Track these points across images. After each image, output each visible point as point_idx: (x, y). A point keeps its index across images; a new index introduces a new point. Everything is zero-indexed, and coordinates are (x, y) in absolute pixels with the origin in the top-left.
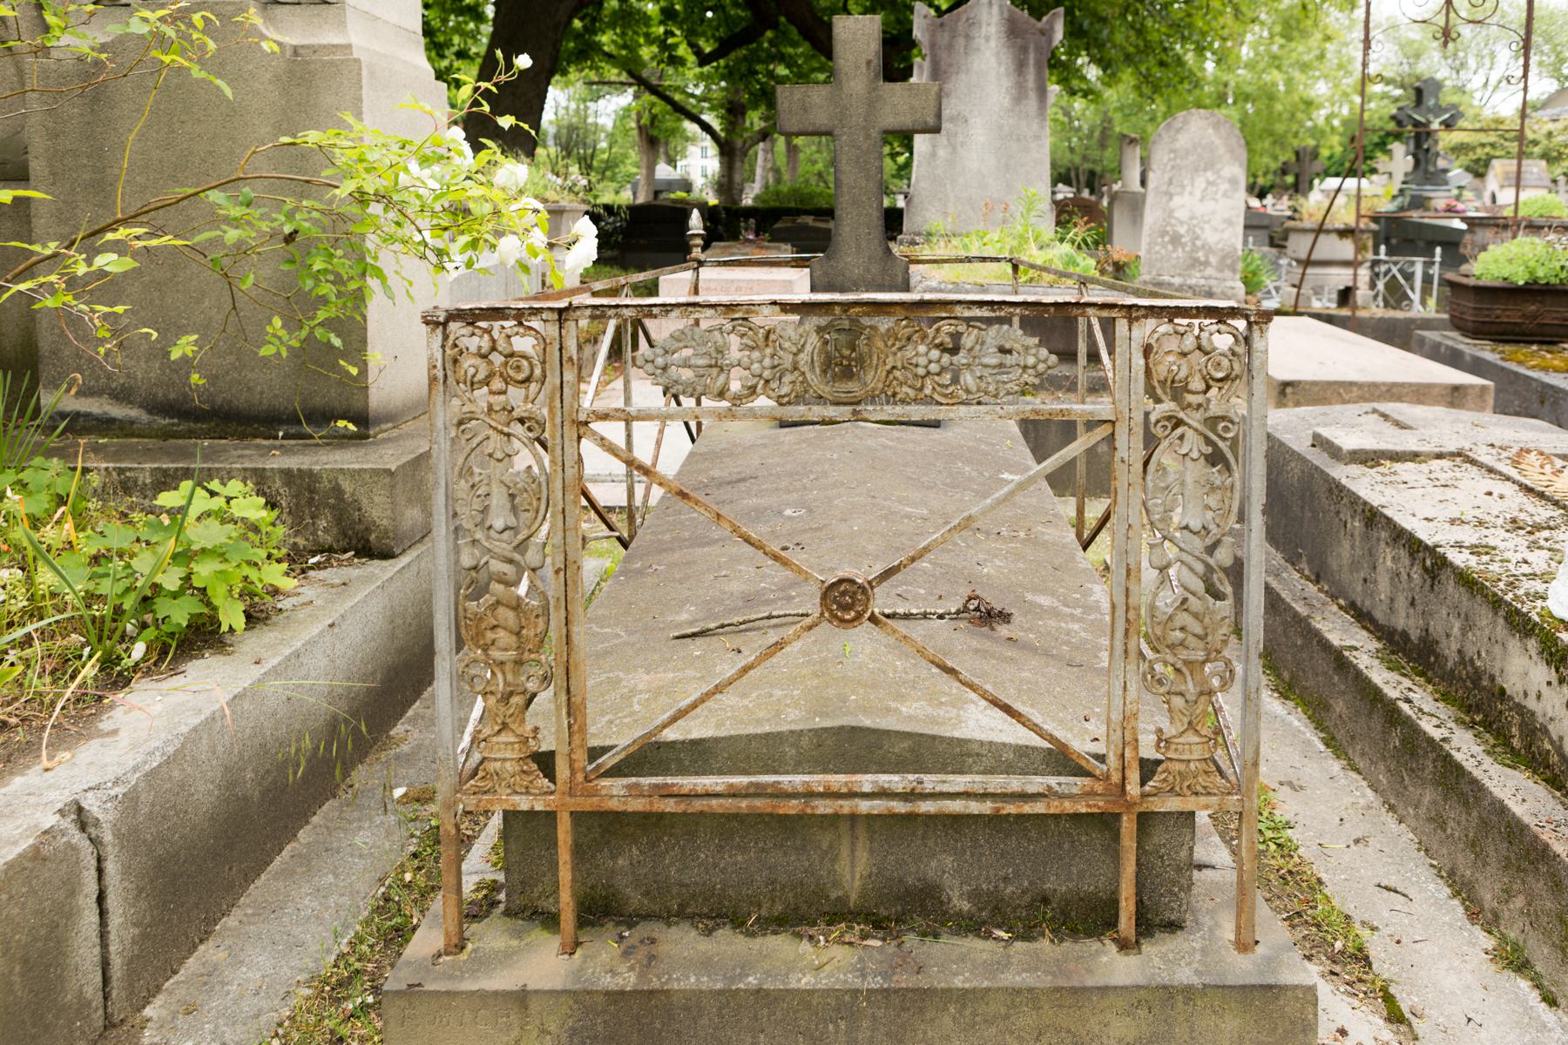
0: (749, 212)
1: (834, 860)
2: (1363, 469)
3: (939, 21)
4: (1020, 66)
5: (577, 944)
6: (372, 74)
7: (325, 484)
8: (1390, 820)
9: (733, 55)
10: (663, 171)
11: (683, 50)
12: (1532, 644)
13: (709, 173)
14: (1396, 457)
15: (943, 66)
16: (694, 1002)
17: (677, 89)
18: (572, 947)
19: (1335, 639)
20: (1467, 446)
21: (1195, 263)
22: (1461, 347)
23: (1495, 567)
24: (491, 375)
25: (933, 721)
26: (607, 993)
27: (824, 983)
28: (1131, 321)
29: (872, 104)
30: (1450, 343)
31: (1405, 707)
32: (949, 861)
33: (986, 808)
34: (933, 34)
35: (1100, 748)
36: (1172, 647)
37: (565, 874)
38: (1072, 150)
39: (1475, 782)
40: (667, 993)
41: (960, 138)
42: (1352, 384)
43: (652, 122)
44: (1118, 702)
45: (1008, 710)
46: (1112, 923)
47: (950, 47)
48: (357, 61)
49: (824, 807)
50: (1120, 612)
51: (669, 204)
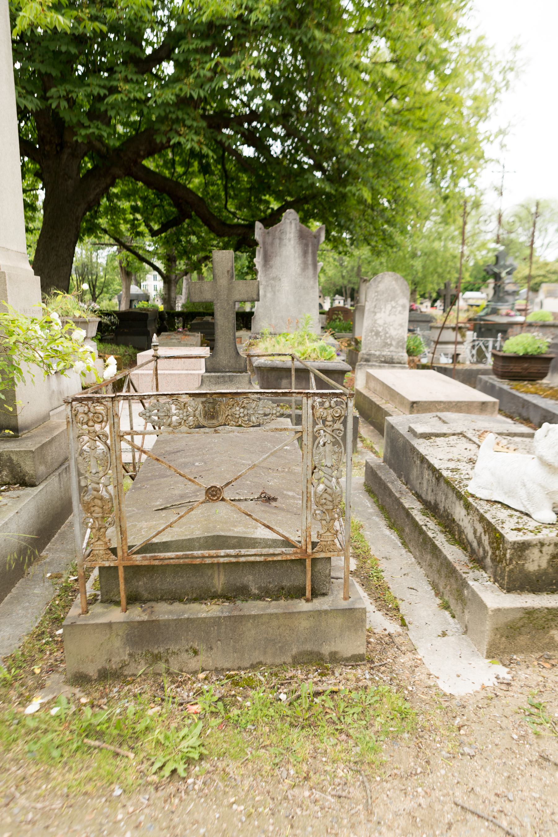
0: (179, 314)
1: (213, 579)
2: (424, 440)
3: (266, 231)
4: (305, 253)
5: (127, 609)
6: (10, 278)
7: (5, 457)
8: (418, 568)
9: (169, 232)
10: (134, 289)
11: (142, 228)
12: (462, 502)
13: (158, 289)
14: (437, 435)
15: (269, 253)
16: (167, 623)
17: (140, 248)
18: (126, 610)
19: (407, 506)
20: (465, 430)
21: (386, 345)
22: (495, 383)
23: (457, 476)
24: (89, 420)
25: (245, 533)
26: (138, 622)
27: (209, 615)
28: (308, 398)
29: (230, 289)
30: (491, 381)
31: (424, 527)
32: (251, 578)
33: (262, 559)
34: (264, 238)
35: (299, 539)
36: (322, 505)
37: (122, 587)
38: (343, 277)
39: (440, 550)
40: (158, 621)
41: (277, 288)
42: (441, 402)
43: (128, 265)
44: (304, 523)
45: (268, 527)
46: (304, 595)
47: (272, 244)
48: (4, 273)
49: (208, 561)
50: (305, 494)
51: (138, 311)
